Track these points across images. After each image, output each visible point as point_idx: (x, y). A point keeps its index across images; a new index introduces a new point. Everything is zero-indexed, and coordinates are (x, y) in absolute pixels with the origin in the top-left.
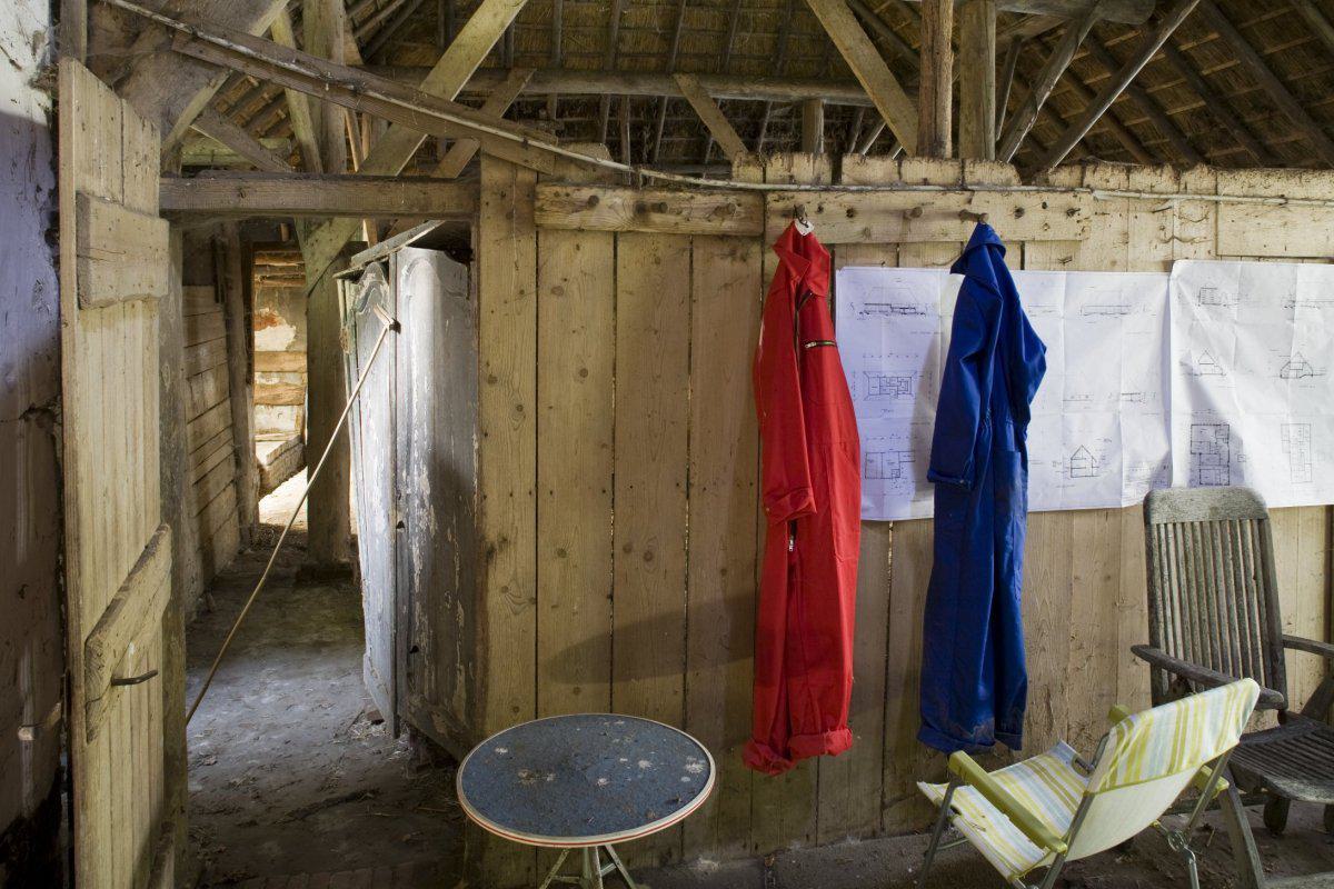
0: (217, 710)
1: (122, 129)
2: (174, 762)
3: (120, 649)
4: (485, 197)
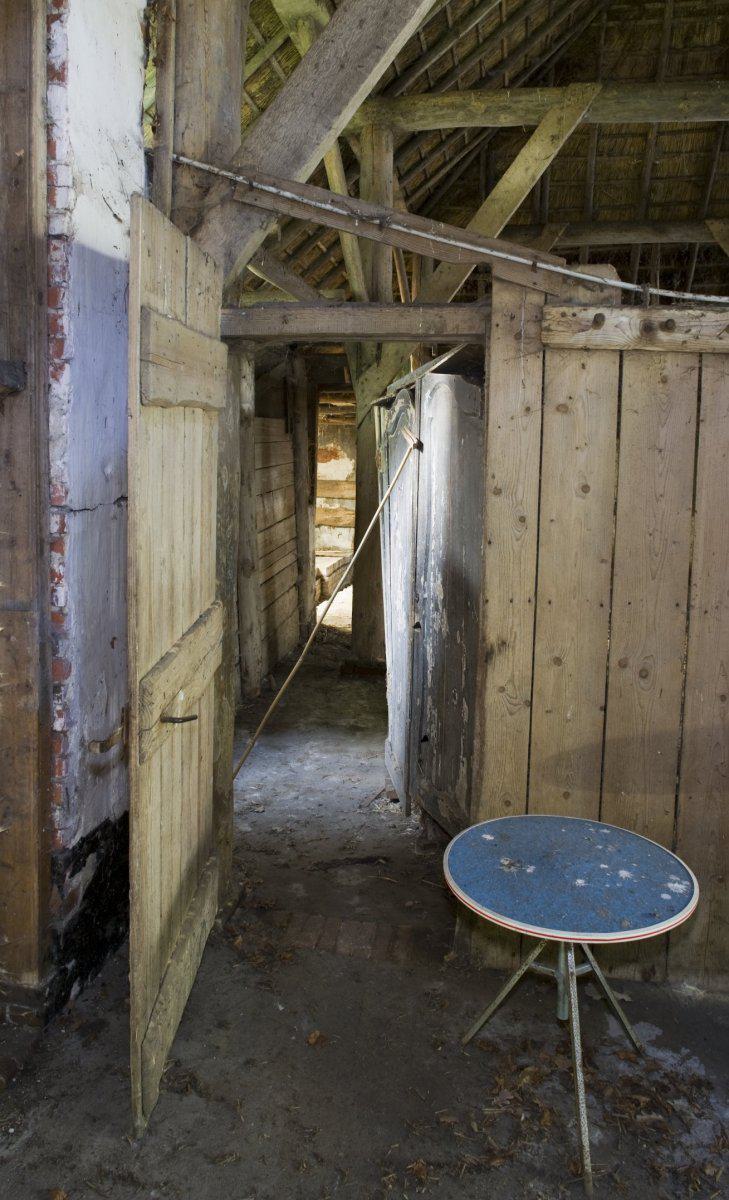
0: (269, 770)
1: (187, 261)
2: (221, 800)
3: (169, 693)
4: (496, 319)
